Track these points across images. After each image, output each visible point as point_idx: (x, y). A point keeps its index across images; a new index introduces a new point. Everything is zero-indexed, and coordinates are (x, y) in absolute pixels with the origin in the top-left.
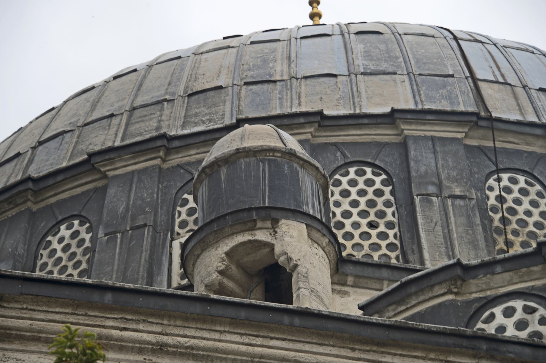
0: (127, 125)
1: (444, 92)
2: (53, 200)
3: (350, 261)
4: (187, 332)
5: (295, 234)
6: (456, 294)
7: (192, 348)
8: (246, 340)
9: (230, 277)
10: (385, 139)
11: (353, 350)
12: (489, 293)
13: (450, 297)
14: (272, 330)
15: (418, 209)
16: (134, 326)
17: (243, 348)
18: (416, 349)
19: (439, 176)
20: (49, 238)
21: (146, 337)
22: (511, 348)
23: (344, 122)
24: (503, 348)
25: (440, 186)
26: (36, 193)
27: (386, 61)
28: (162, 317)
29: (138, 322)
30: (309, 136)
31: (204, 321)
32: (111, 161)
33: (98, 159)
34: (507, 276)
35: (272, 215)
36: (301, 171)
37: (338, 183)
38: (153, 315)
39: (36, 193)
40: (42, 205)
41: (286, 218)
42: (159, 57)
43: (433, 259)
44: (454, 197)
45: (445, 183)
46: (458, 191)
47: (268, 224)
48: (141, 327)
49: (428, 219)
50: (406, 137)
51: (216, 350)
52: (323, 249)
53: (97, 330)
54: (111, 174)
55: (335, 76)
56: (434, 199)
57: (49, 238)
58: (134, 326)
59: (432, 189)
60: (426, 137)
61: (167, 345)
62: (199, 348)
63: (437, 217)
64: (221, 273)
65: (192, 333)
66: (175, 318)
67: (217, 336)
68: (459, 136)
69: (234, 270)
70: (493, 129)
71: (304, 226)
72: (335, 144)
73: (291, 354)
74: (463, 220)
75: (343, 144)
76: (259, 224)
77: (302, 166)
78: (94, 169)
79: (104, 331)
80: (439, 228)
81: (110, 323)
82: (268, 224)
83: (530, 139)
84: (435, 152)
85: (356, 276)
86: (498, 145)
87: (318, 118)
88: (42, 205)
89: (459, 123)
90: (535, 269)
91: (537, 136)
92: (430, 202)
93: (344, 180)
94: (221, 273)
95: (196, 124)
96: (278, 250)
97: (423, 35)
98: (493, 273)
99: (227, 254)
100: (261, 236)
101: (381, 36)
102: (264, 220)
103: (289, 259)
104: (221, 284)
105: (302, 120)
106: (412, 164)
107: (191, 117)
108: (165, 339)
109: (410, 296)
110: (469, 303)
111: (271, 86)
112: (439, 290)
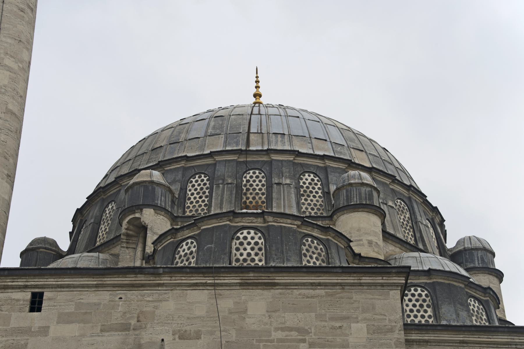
0: (133, 163)
1: (235, 140)
2: (109, 194)
3: (178, 217)
4: (35, 280)
5: (148, 213)
6: (174, 238)
7: (36, 285)
8: (56, 280)
9: (130, 230)
10: (210, 162)
11: (94, 278)
12: (183, 237)
13: (172, 240)
14: (65, 275)
15: (214, 190)
16: (16, 280)
17: (54, 283)
18: (115, 275)
19: (224, 175)
20: (192, 179)
21: (20, 283)
22: (147, 270)
23: (195, 158)
24: (144, 270)
25: (224, 180)
26: (104, 192)
27: (219, 129)
28: (26, 276)
29: (18, 279)
30: (183, 165)
31: (41, 276)
32: (122, 180)
33: (118, 180)
34: (187, 231)
35: (140, 208)
36: (157, 188)
37: (192, 182)
38: (23, 276)
39: (104, 192)
40: (106, 196)
41: (145, 208)
42: (167, 126)
43: (215, 210)
44: (228, 184)
45: (226, 178)
46: (230, 181)
47: (139, 211)
48: (19, 280)
49: (217, 194)
50: (217, 161)
51: (45, 285)
52: (163, 216)
53: (3, 283)
54: (123, 184)
55: (199, 138)
56: (221, 185)
57: (192, 179)
58: (16, 280)
59: (221, 181)
60: (224, 160)
61: (28, 285)
62: (39, 285)
63: (220, 192)
64: (126, 229)
65: (37, 280)
66: (31, 276)
67: (45, 280)
68: (235, 158)
69: (131, 227)
70: (246, 154)
71: (152, 210)
72: (193, 167)
73: (71, 282)
74: (229, 193)
75: (196, 166)
76: (136, 211)
77: (157, 186)
78: (118, 183)
79: (6, 283)
80: (220, 197)
81: (8, 280)
82: (139, 211)
83: (262, 156)
84: (225, 166)
85: (181, 222)
86: (248, 159)
87: (101, 190)
88: (106, 196)
89: (235, 154)
90: (195, 228)
91: (264, 155)
92: (219, 187)
93: (194, 180)
94: (126, 229)
95: (151, 162)
96: (142, 220)
97: (239, 115)
98: (184, 231)
99: (127, 222)
100: (137, 215)
101: (223, 118)
102: (138, 209)
103: (145, 223)
104: (127, 233)
105: (180, 159)
106: (216, 172)
107: (152, 159)
108: (27, 283)
109: (162, 240)
110: (177, 241)
111: (177, 144)
112: (169, 238)
